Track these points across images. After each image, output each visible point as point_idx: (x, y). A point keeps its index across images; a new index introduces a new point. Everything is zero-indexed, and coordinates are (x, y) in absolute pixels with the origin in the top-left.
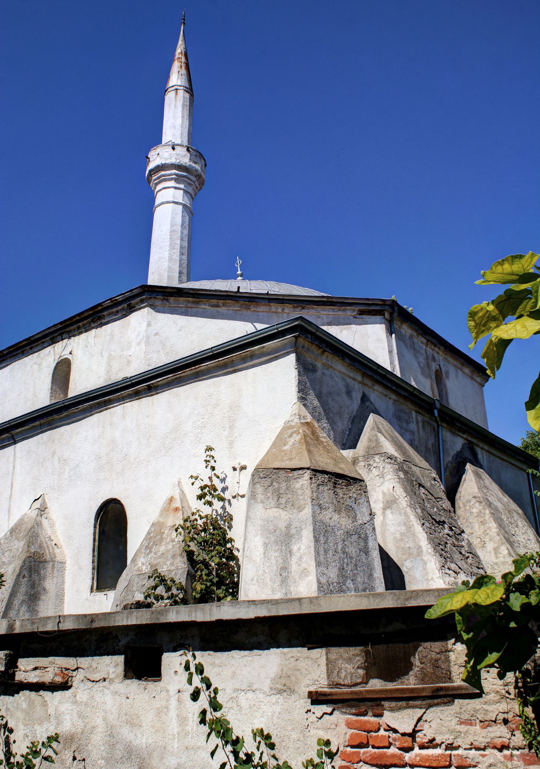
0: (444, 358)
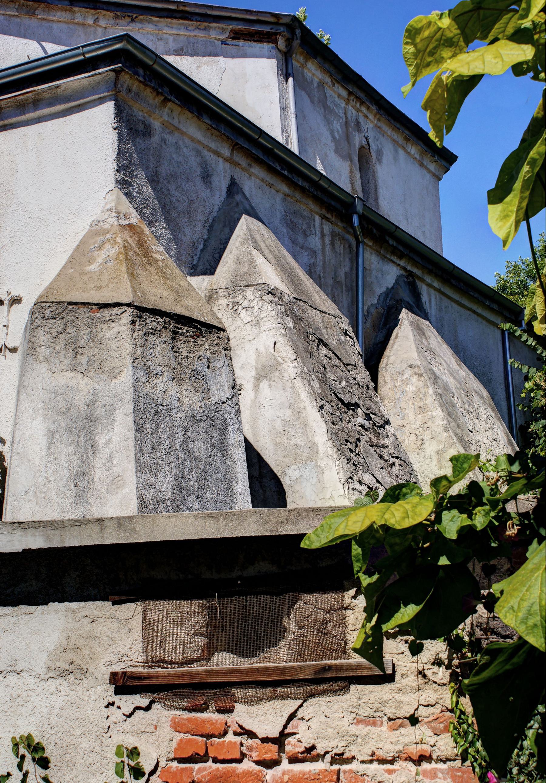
0: (376, 125)
